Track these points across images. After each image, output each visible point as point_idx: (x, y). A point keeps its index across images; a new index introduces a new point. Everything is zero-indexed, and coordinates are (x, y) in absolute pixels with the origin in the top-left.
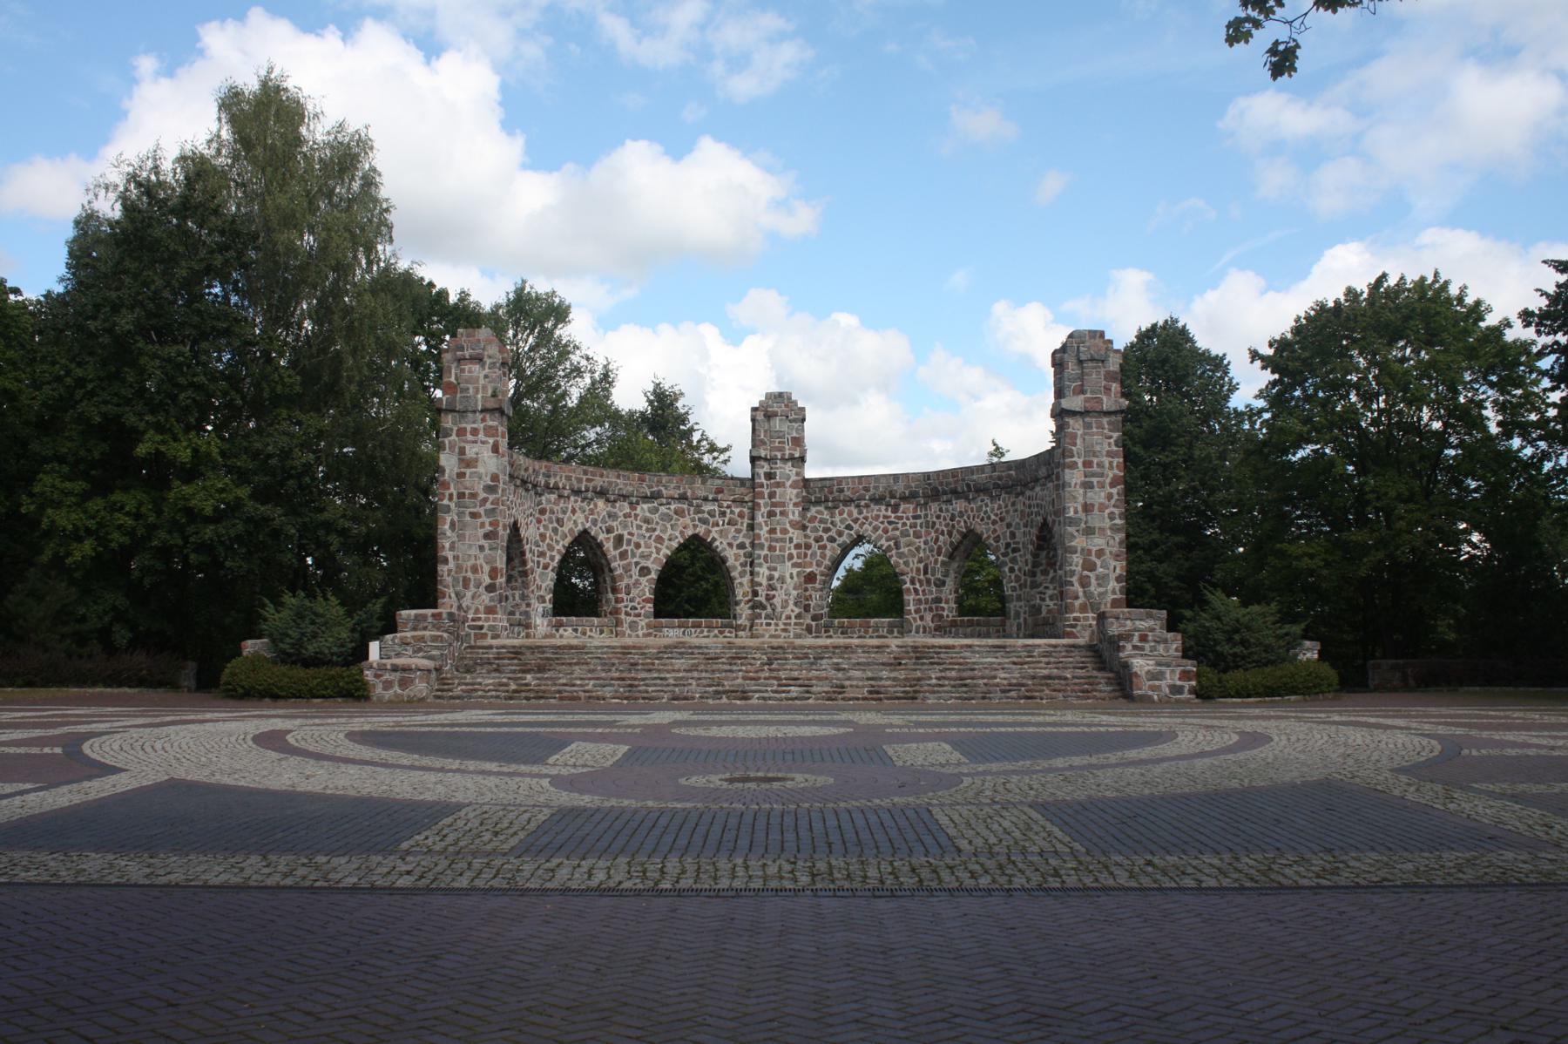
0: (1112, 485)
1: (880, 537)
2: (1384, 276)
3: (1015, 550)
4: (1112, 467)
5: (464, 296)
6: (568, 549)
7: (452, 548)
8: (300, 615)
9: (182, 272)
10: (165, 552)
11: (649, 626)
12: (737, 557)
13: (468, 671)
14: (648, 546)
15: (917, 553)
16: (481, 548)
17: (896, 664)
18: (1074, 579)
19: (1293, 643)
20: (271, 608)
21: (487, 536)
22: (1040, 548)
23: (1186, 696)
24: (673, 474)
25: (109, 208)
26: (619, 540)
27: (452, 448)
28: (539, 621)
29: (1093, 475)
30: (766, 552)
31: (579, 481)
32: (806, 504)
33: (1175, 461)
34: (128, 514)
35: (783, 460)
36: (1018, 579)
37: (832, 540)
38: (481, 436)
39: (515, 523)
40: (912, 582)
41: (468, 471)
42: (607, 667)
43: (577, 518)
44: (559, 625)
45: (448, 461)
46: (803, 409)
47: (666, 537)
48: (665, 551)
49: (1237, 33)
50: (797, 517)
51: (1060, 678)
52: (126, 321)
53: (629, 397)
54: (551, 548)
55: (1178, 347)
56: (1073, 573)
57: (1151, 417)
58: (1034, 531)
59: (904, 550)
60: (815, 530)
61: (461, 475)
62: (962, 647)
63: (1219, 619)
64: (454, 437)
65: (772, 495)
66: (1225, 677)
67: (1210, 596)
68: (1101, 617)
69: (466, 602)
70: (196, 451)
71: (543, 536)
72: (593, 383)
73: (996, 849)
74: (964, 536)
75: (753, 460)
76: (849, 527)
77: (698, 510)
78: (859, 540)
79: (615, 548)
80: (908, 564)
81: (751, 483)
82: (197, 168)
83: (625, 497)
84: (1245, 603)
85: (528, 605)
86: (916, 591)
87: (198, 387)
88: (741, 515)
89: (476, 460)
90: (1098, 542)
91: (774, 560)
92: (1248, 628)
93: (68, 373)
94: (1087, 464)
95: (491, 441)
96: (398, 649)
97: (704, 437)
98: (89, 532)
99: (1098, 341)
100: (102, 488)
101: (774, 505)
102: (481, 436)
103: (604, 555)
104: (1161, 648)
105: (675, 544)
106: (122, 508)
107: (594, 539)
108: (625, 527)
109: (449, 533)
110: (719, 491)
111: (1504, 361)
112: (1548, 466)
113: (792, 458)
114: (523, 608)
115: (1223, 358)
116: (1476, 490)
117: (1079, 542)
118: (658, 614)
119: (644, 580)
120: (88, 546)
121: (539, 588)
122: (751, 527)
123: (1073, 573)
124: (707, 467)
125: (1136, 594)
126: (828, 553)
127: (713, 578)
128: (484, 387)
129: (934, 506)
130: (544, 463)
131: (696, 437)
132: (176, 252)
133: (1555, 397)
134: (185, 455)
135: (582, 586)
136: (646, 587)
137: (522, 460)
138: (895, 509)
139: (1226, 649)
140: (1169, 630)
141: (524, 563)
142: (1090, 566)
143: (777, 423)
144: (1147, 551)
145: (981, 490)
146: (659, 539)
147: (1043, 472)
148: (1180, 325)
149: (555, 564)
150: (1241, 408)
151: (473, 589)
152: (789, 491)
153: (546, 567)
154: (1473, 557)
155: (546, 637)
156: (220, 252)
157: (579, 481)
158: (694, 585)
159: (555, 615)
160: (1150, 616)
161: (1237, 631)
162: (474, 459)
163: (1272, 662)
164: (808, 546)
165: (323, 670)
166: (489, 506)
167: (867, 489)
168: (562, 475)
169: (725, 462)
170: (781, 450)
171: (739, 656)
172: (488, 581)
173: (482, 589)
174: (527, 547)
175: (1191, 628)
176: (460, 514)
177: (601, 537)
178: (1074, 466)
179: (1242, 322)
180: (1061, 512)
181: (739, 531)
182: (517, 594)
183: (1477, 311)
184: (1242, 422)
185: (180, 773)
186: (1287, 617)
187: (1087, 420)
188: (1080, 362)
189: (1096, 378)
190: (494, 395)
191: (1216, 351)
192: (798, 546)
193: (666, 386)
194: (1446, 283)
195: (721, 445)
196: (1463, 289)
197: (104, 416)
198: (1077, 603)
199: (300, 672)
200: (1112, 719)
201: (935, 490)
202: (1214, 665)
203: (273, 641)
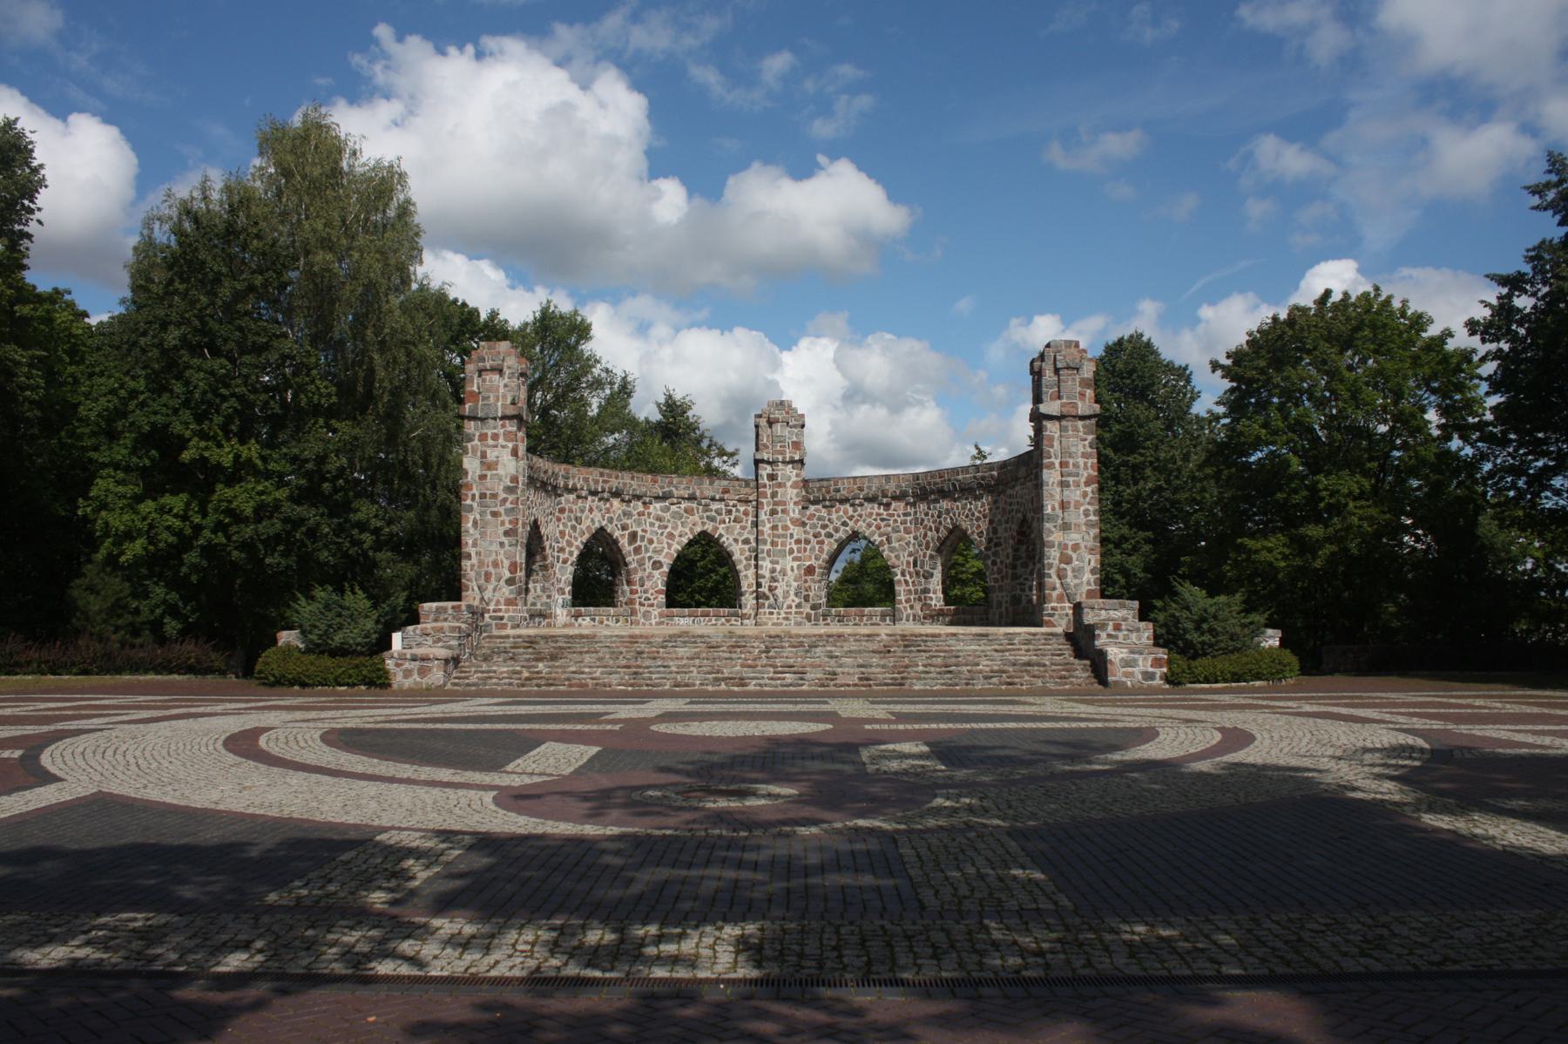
0: (1087, 484)
1: (873, 534)
2: (1328, 293)
3: (996, 545)
4: (1086, 466)
5: (494, 315)
6: (586, 545)
7: (475, 545)
8: (327, 607)
9: (225, 292)
10: (209, 551)
11: (661, 615)
13: (486, 659)
14: (660, 542)
15: (903, 542)
16: (502, 544)
17: (887, 651)
19: (1257, 631)
20: (303, 602)
21: (506, 533)
22: (1020, 542)
23: (1158, 682)
24: (684, 475)
25: (162, 235)
26: (633, 536)
27: (474, 452)
28: (559, 611)
31: (596, 482)
32: (807, 502)
33: (1143, 463)
34: (176, 516)
36: (1000, 571)
37: (829, 535)
38: (501, 441)
39: (536, 521)
40: (903, 574)
41: (489, 473)
42: (616, 655)
43: (594, 516)
44: (576, 616)
45: (471, 464)
47: (676, 533)
48: (677, 547)
50: (797, 515)
51: (1039, 665)
52: (172, 337)
53: (645, 408)
54: (569, 544)
55: (1143, 358)
56: (1051, 566)
57: (1119, 422)
58: (1015, 527)
59: (895, 544)
60: (814, 526)
61: (482, 477)
62: (948, 635)
63: (1188, 608)
64: (476, 442)
65: (774, 495)
66: (1193, 664)
67: (1179, 588)
68: (1078, 608)
70: (237, 457)
71: (562, 533)
73: (967, 905)
74: (951, 532)
76: (845, 524)
79: (630, 543)
82: (239, 200)
83: (638, 498)
84: (1211, 595)
85: (549, 597)
86: (906, 582)
87: (240, 398)
88: (746, 513)
89: (497, 463)
90: (1074, 537)
92: (1215, 617)
95: (510, 445)
96: (420, 640)
98: (140, 533)
99: (1073, 350)
100: (152, 491)
101: (776, 504)
103: (620, 551)
104: (1134, 636)
105: (685, 540)
106: (171, 510)
107: (611, 535)
108: (639, 524)
109: (472, 531)
110: (726, 491)
111: (1447, 370)
112: (1487, 467)
113: (792, 462)
114: (544, 599)
115: (1186, 368)
116: (1419, 488)
118: (670, 603)
119: (656, 573)
120: (140, 543)
121: (559, 581)
122: (756, 524)
123: (1051, 566)
124: (717, 470)
125: (1109, 586)
126: (826, 548)
127: (723, 570)
128: (504, 396)
129: (923, 506)
130: (564, 466)
132: (220, 273)
133: (1493, 400)
134: (227, 461)
135: (599, 576)
136: (658, 580)
138: (887, 506)
139: (1194, 637)
140: (1141, 620)
141: (545, 558)
142: (1066, 560)
143: (778, 428)
144: (1117, 546)
145: (943, 494)
146: (671, 536)
148: (1145, 339)
149: (574, 558)
150: (1204, 414)
152: (790, 490)
153: (565, 562)
154: (1414, 549)
155: (565, 626)
156: (261, 273)
157: (596, 482)
158: (703, 578)
159: (574, 605)
160: (1123, 606)
161: (1204, 620)
162: (493, 461)
163: (1238, 650)
165: (347, 659)
166: (508, 505)
167: (861, 489)
168: (579, 476)
171: (739, 644)
172: (507, 575)
173: (502, 582)
174: (547, 544)
175: (1161, 617)
176: (482, 513)
177: (617, 534)
179: (1203, 340)
180: (1041, 508)
181: (743, 528)
183: (1419, 322)
184: (1202, 428)
185: (115, 788)
186: (1249, 607)
187: (1064, 423)
188: (1057, 371)
189: (1072, 384)
190: (513, 403)
191: (1179, 361)
192: (798, 542)
193: (678, 396)
194: (1390, 298)
195: (729, 449)
196: (1405, 302)
197: (153, 424)
198: (1055, 594)
199: (327, 661)
200: (1091, 709)
201: (923, 489)
202: (1182, 652)
203: (303, 632)
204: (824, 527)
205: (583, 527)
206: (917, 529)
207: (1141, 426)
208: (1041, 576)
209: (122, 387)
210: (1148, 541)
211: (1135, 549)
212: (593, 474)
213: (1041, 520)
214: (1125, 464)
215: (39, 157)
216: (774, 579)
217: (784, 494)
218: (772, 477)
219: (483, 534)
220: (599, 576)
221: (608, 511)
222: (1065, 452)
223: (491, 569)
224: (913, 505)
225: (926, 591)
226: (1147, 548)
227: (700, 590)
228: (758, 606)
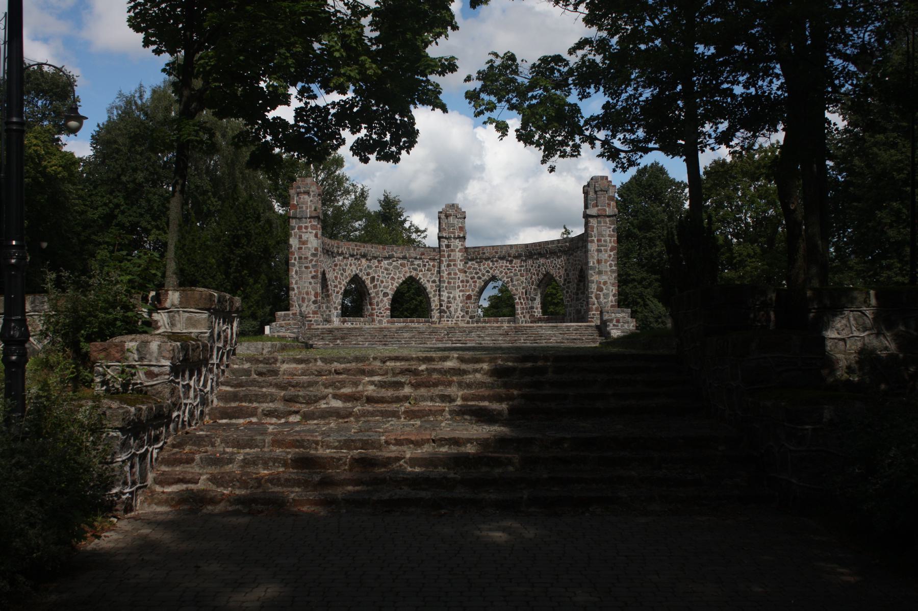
0: (611, 251)
3: (569, 282)
4: (610, 241)
7: (296, 283)
11: (388, 322)
12: (432, 287)
15: (521, 282)
16: (310, 283)
17: (506, 334)
18: (593, 296)
21: (313, 277)
22: (580, 281)
24: (399, 245)
26: (373, 279)
27: (295, 235)
28: (335, 319)
29: (602, 246)
30: (446, 284)
31: (353, 250)
32: (466, 260)
35: (455, 238)
36: (570, 297)
37: (479, 278)
38: (309, 230)
40: (520, 299)
43: (352, 268)
44: (344, 322)
45: (294, 242)
46: (464, 212)
49: (544, 162)
50: (462, 267)
54: (340, 283)
60: (471, 273)
61: (300, 248)
65: (449, 256)
69: (303, 309)
71: (336, 277)
72: (356, 198)
74: (545, 276)
75: (439, 238)
76: (488, 272)
77: (412, 264)
78: (494, 278)
80: (518, 290)
81: (439, 250)
83: (375, 258)
88: (434, 266)
90: (604, 278)
91: (450, 289)
93: (110, 202)
94: (599, 241)
97: (412, 225)
99: (605, 181)
101: (450, 261)
102: (309, 230)
104: (626, 326)
105: (401, 281)
107: (361, 278)
108: (376, 272)
110: (423, 254)
113: (459, 237)
114: (328, 313)
117: (595, 278)
119: (385, 299)
122: (439, 272)
124: (414, 241)
126: (478, 285)
127: (419, 299)
129: (530, 262)
131: (407, 225)
135: (357, 300)
136: (387, 302)
137: (327, 240)
138: (511, 262)
141: (328, 291)
142: (600, 289)
143: (451, 219)
145: (541, 255)
146: (393, 279)
147: (580, 244)
149: (342, 291)
151: (306, 302)
153: (338, 293)
157: (353, 250)
158: (410, 301)
160: (623, 312)
161: (660, 317)
162: (306, 239)
164: (467, 282)
166: (314, 263)
167: (497, 253)
168: (345, 247)
169: (424, 237)
170: (453, 233)
172: (313, 299)
177: (364, 278)
178: (593, 241)
180: (587, 263)
181: (432, 274)
182: (324, 306)
188: (596, 192)
189: (603, 199)
190: (315, 210)
192: (462, 282)
193: (391, 197)
195: (422, 228)
198: (594, 307)
201: (530, 252)
204: (477, 273)
205: (347, 274)
206: (527, 274)
207: (653, 217)
208: (588, 298)
209: (110, 202)
210: (657, 280)
211: (650, 285)
212: (352, 245)
213: (587, 269)
214: (645, 237)
215: (78, 91)
216: (449, 302)
217: (455, 256)
218: (448, 246)
219: (300, 278)
220: (357, 300)
221: (360, 265)
222: (600, 234)
223: (305, 296)
224: (525, 261)
225: (532, 308)
226: (657, 284)
227: (407, 310)
228: (441, 317)
